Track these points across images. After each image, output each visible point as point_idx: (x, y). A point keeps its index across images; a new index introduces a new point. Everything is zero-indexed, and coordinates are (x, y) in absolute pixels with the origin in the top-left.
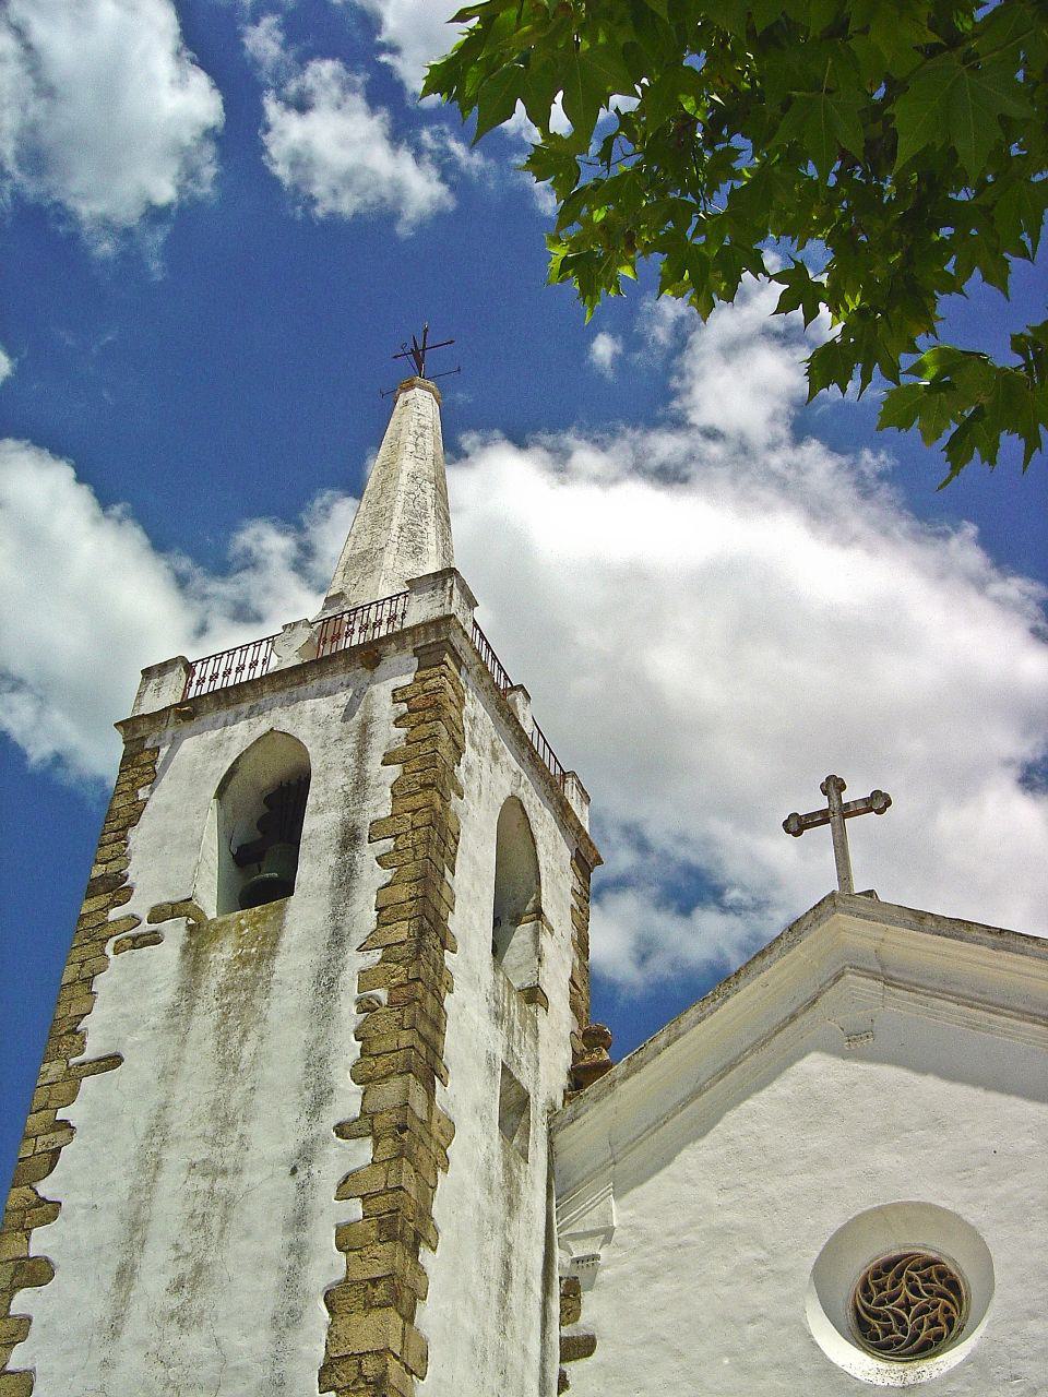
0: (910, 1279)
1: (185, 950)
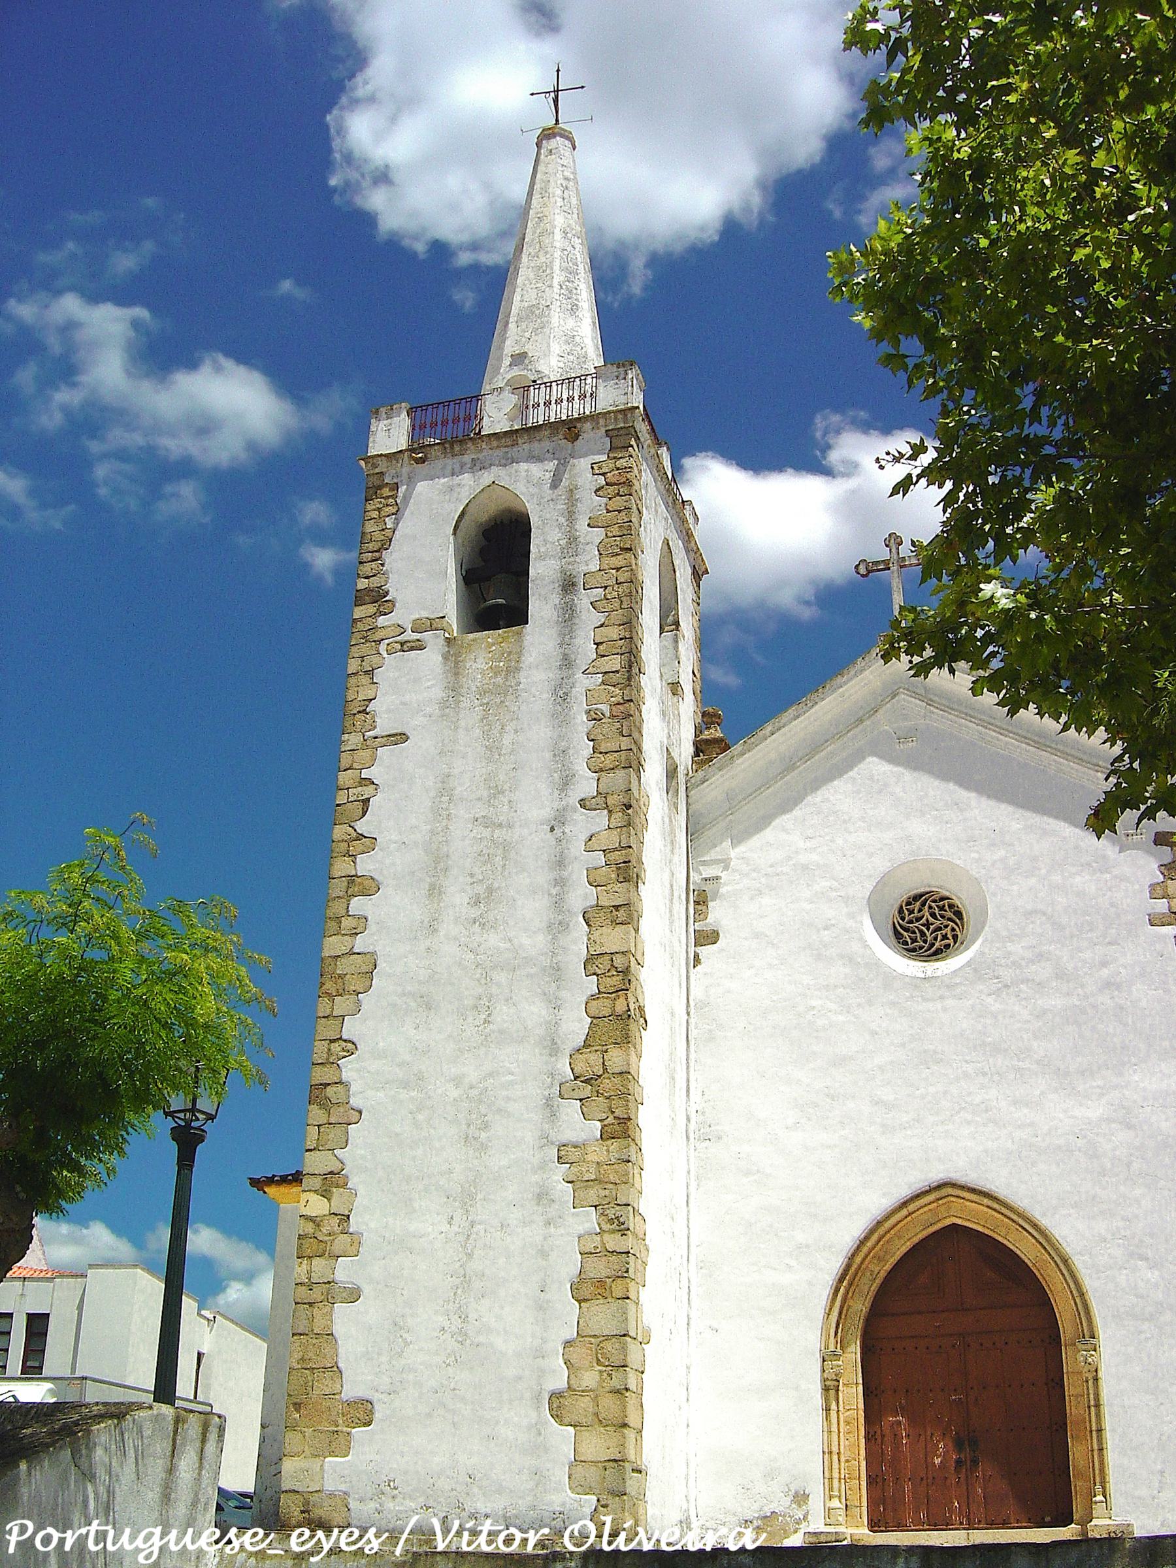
0: (930, 907)
1: (446, 657)
